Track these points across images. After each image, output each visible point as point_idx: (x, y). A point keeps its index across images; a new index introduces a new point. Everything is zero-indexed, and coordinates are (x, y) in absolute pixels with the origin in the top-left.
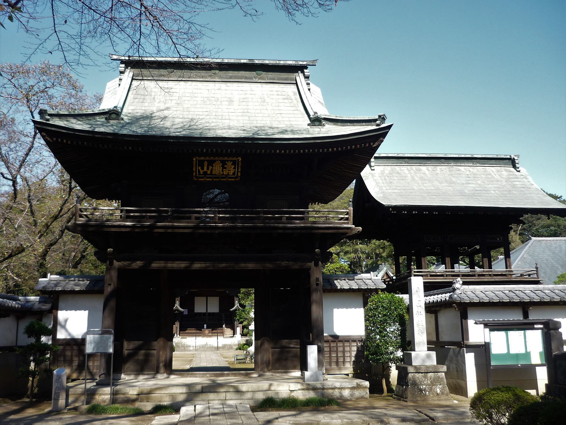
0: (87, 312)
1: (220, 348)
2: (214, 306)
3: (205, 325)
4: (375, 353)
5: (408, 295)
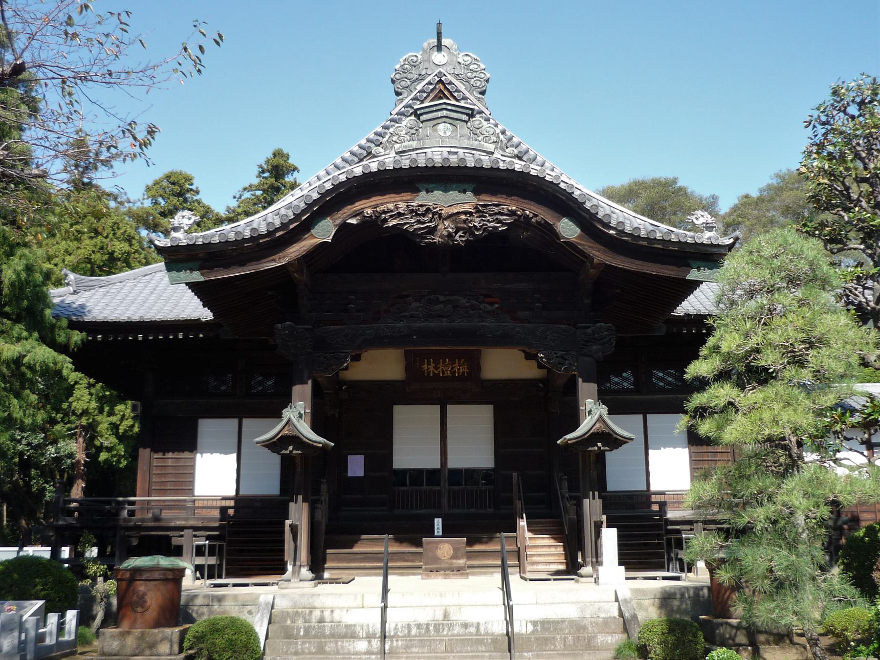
0: (349, 475)
1: (526, 639)
2: (470, 441)
3: (438, 523)
4: (46, 204)
5: (441, 534)
